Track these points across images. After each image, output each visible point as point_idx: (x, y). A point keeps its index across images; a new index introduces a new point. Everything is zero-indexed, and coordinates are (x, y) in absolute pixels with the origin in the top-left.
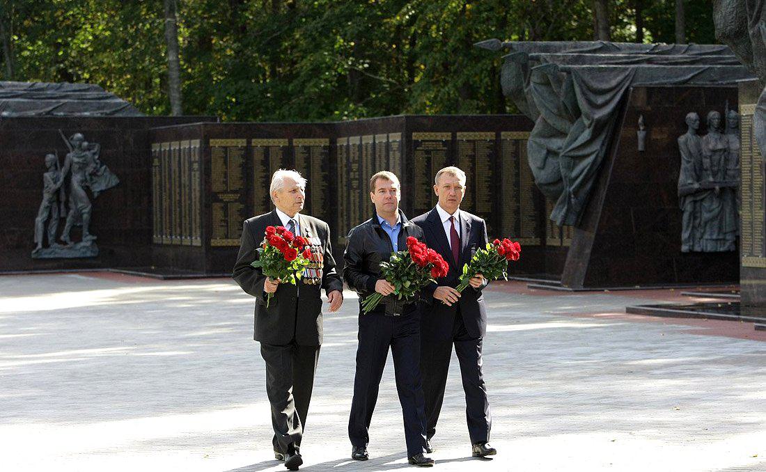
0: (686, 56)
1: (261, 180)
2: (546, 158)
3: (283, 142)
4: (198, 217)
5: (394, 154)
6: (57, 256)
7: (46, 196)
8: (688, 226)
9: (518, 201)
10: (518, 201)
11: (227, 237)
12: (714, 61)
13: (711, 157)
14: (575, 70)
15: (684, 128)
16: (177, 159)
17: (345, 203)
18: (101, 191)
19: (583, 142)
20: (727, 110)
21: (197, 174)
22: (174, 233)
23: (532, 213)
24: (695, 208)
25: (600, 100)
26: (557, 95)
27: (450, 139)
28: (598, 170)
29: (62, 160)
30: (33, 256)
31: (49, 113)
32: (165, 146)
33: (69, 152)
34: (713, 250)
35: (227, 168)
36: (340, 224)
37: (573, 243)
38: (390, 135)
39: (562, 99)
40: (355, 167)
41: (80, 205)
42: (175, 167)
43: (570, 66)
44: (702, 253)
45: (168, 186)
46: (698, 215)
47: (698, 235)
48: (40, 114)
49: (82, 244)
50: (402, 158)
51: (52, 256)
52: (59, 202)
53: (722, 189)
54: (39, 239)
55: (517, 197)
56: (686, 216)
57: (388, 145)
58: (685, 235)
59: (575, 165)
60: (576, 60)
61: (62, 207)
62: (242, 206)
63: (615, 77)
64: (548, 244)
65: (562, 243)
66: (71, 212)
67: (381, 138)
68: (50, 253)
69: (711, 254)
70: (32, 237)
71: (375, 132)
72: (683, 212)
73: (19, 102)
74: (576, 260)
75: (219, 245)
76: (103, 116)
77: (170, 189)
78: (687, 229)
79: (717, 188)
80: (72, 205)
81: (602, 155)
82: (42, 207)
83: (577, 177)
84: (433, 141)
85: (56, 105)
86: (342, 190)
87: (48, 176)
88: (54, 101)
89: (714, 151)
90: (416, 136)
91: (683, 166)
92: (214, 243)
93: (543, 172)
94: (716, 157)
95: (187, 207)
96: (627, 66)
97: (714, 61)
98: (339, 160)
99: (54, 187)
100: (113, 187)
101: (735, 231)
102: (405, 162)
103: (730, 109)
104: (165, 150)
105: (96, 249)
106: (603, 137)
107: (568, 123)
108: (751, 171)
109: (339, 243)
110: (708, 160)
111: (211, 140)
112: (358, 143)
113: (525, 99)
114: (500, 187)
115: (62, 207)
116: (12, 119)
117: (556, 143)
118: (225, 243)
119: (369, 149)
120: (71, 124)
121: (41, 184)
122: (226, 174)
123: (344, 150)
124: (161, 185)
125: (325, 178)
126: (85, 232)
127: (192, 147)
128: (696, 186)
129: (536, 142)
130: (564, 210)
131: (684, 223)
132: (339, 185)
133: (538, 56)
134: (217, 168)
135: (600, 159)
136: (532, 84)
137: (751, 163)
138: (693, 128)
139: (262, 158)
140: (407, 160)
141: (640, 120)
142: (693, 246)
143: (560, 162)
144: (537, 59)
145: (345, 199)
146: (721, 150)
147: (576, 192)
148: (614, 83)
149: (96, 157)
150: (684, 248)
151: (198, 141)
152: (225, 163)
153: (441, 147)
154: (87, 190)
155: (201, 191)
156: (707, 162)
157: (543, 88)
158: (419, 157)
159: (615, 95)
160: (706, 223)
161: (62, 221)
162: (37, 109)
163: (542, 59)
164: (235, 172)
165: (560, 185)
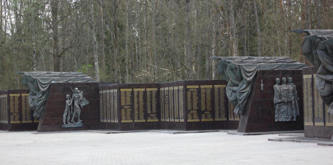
0: (274, 60)
1: (137, 102)
2: (232, 93)
3: (143, 90)
4: (117, 113)
5: (181, 93)
6: (70, 127)
7: (66, 108)
8: (277, 114)
9: (220, 107)
10: (220, 107)
11: (126, 120)
12: (284, 62)
13: (284, 92)
14: (241, 66)
15: (275, 83)
16: (109, 95)
17: (163, 109)
18: (84, 106)
19: (244, 88)
20: (288, 77)
21: (116, 100)
22: (108, 119)
23: (224, 110)
24: (279, 108)
25: (249, 75)
26: (235, 74)
27: (198, 87)
28: (249, 97)
29: (71, 96)
30: (63, 127)
31: (67, 82)
32: (104, 92)
33: (73, 94)
34: (285, 121)
35: (126, 98)
36: (162, 115)
37: (243, 121)
38: (179, 87)
39: (237, 74)
40: (167, 97)
41: (77, 110)
42: (108, 97)
43: (239, 64)
44: (281, 122)
45: (105, 104)
46: (280, 110)
47: (280, 116)
48: (64, 82)
49: (78, 123)
50: (183, 94)
51: (68, 127)
52: (70, 109)
53: (287, 102)
54: (64, 121)
55: (219, 106)
56: (276, 110)
57: (178, 90)
58: (276, 116)
59: (241, 95)
60: (240, 62)
61: (72, 111)
62: (131, 110)
63: (253, 67)
64: (229, 120)
65: (234, 120)
66: (74, 113)
67: (176, 88)
68: (68, 126)
69: (284, 122)
70: (62, 121)
71: (106, 89)
72: (275, 109)
73: (57, 78)
74: (242, 125)
75: (124, 122)
76: (84, 82)
77: (106, 105)
78: (277, 115)
79: (286, 101)
80: (74, 110)
81: (250, 92)
82: (65, 111)
83: (242, 99)
84: (193, 88)
85: (69, 79)
86: (162, 104)
87: (67, 101)
88: (68, 78)
89: (284, 90)
90: (188, 87)
91: (275, 95)
92: (122, 121)
93: (231, 97)
94: (285, 92)
95: (113, 111)
96: (257, 64)
97: (284, 62)
98: (161, 95)
99: (69, 105)
100: (87, 105)
101: (292, 115)
102: (184, 95)
103: (289, 77)
104: (104, 93)
105: (82, 124)
106: (250, 86)
107: (239, 82)
108: (307, 96)
109: (162, 121)
110: (283, 93)
111: (121, 89)
112: (168, 89)
113: (225, 75)
114: (214, 102)
115: (72, 111)
116: (55, 84)
117: (235, 88)
118: (126, 121)
119: (163, 91)
120: (74, 85)
121: (65, 103)
122: (125, 100)
123: (163, 91)
124: (103, 104)
125: (156, 101)
126: (79, 119)
127: (114, 91)
128: (280, 101)
129: (229, 88)
130: (238, 109)
131: (276, 113)
132: (161, 103)
133: (229, 61)
134: (123, 98)
135: (249, 93)
136: (227, 70)
137: (307, 93)
138: (278, 83)
139: (137, 95)
140: (185, 94)
141: (262, 81)
142: (279, 120)
143: (237, 94)
144: (229, 62)
145: (163, 107)
146: (287, 89)
147: (242, 103)
148: (253, 69)
149: (82, 95)
150: (276, 120)
151: (117, 90)
152: (125, 96)
153: (195, 90)
154: (79, 105)
155: (118, 105)
156: (282, 93)
157: (231, 71)
158: (189, 94)
159: (254, 73)
160: (283, 112)
161: (72, 116)
162: (63, 80)
163: (230, 62)
164: (129, 99)
165: (236, 102)
